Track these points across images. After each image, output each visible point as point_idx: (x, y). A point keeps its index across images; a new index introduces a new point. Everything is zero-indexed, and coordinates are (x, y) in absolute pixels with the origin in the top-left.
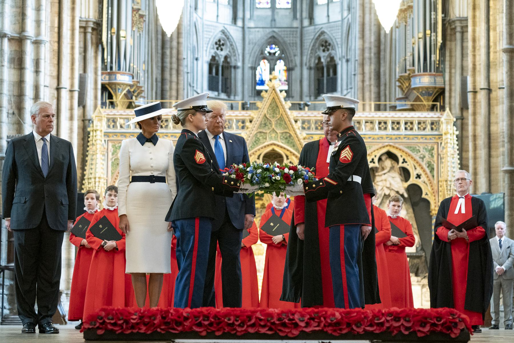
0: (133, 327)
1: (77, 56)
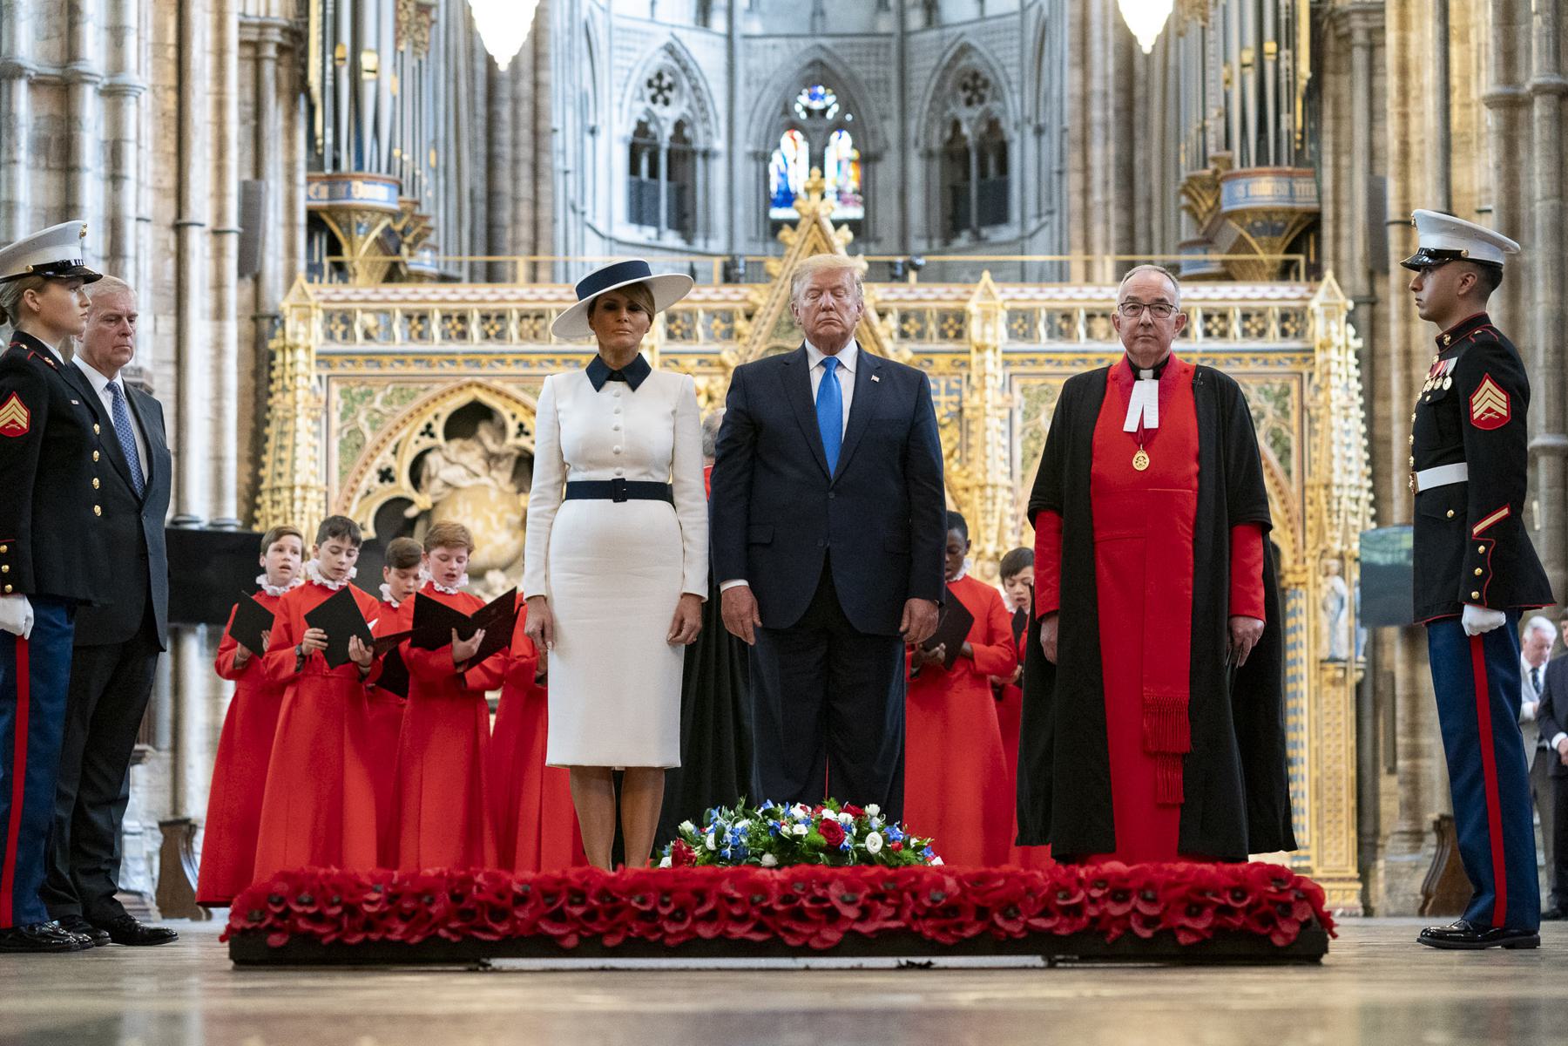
0: (370, 923)
1: (234, 130)
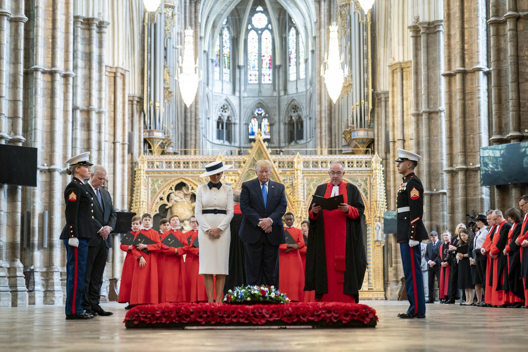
0: (157, 319)
1: (127, 120)
